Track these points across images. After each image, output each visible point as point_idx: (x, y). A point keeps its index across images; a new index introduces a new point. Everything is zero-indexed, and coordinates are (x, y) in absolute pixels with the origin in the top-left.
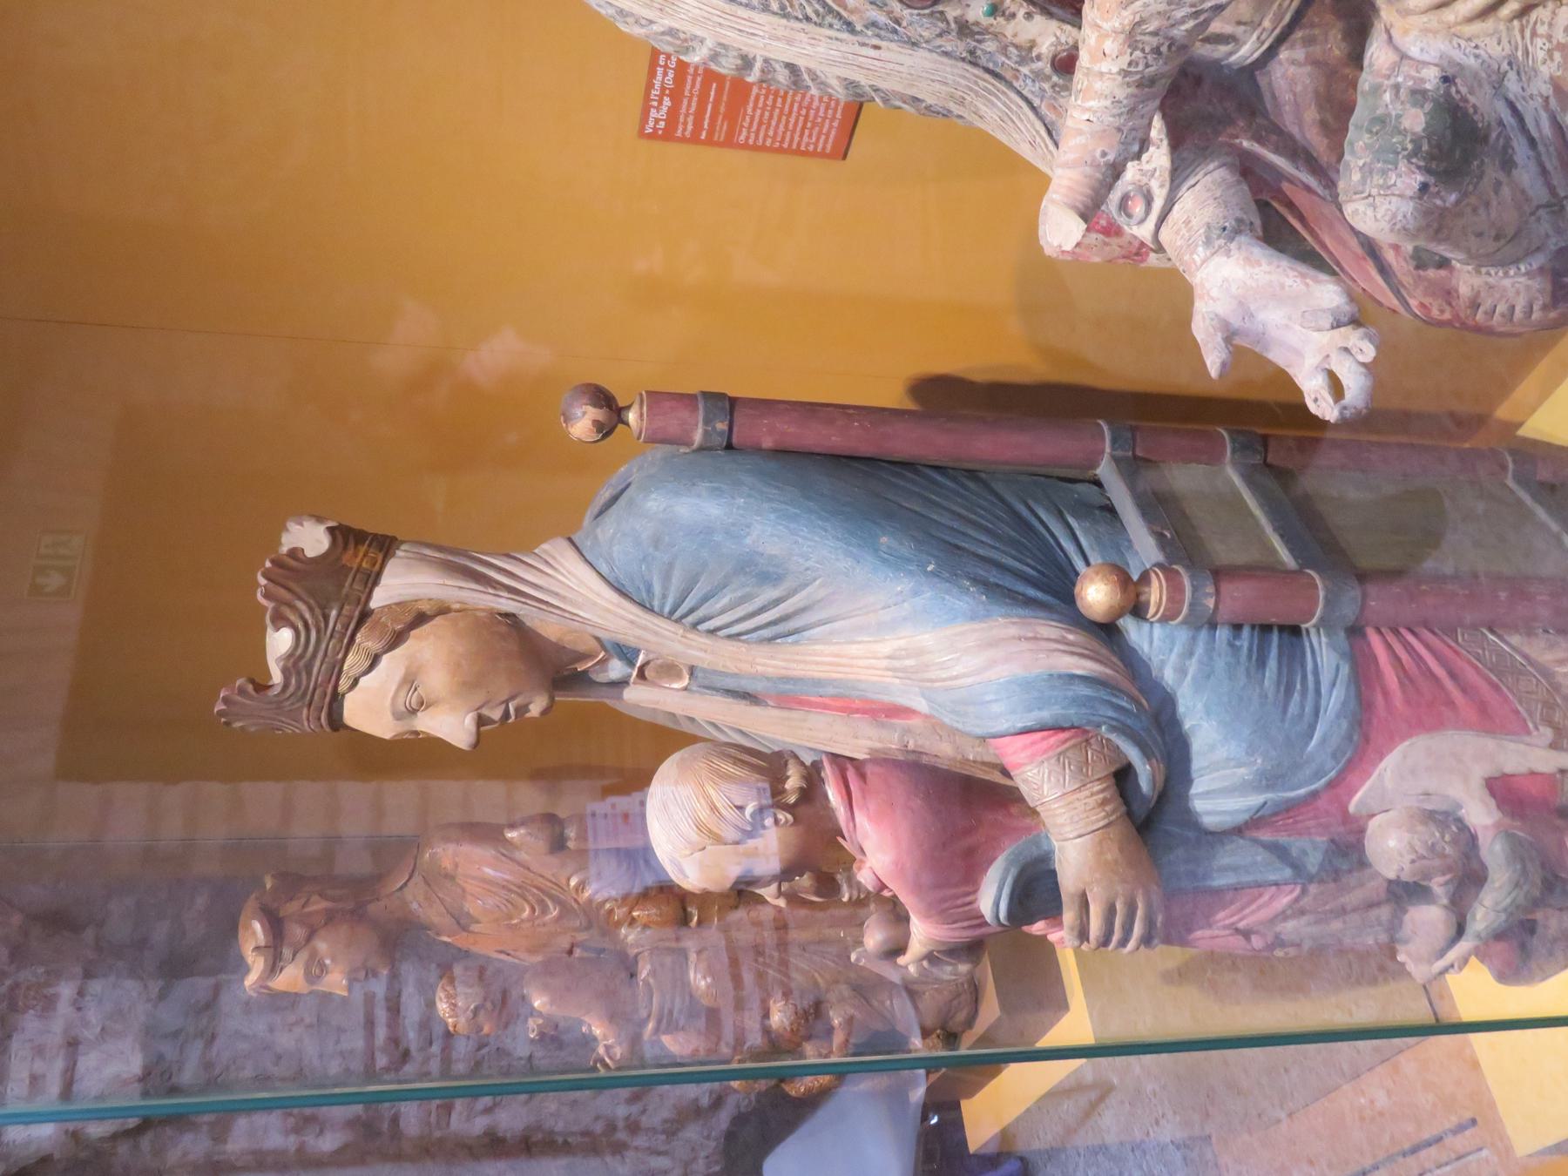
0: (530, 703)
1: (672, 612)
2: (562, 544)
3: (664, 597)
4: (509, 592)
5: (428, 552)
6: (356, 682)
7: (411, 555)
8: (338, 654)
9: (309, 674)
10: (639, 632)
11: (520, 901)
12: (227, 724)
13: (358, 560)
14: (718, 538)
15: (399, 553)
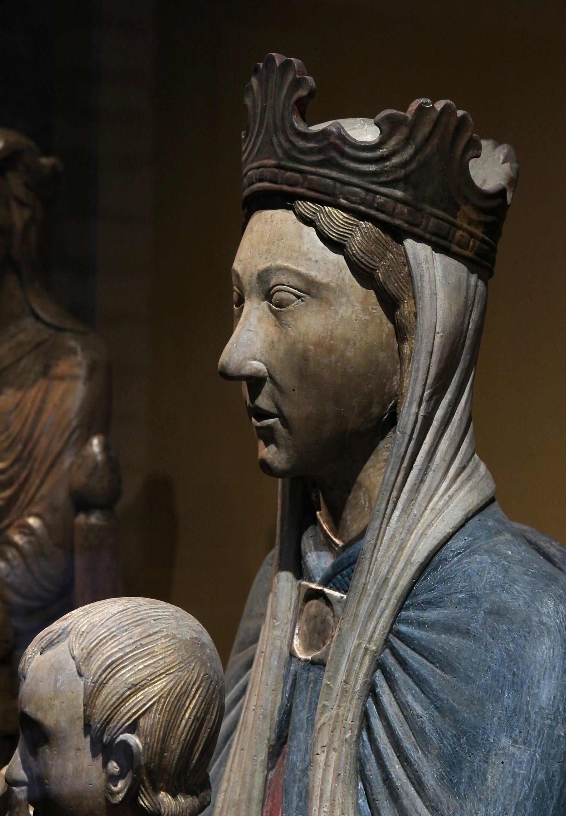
0: (277, 445)
1: (399, 635)
2: (488, 488)
3: (421, 624)
4: (424, 417)
5: (475, 315)
6: (309, 222)
7: (471, 292)
8: (346, 199)
9: (320, 164)
10: (372, 590)
11: (12, 456)
12: (256, 70)
13: (465, 225)
14: (508, 699)
15: (473, 278)
